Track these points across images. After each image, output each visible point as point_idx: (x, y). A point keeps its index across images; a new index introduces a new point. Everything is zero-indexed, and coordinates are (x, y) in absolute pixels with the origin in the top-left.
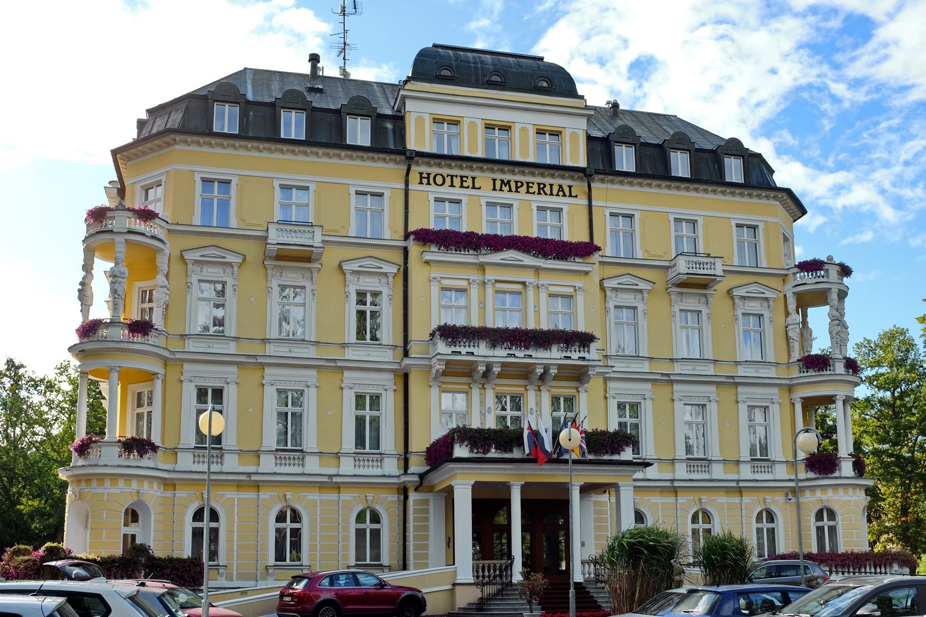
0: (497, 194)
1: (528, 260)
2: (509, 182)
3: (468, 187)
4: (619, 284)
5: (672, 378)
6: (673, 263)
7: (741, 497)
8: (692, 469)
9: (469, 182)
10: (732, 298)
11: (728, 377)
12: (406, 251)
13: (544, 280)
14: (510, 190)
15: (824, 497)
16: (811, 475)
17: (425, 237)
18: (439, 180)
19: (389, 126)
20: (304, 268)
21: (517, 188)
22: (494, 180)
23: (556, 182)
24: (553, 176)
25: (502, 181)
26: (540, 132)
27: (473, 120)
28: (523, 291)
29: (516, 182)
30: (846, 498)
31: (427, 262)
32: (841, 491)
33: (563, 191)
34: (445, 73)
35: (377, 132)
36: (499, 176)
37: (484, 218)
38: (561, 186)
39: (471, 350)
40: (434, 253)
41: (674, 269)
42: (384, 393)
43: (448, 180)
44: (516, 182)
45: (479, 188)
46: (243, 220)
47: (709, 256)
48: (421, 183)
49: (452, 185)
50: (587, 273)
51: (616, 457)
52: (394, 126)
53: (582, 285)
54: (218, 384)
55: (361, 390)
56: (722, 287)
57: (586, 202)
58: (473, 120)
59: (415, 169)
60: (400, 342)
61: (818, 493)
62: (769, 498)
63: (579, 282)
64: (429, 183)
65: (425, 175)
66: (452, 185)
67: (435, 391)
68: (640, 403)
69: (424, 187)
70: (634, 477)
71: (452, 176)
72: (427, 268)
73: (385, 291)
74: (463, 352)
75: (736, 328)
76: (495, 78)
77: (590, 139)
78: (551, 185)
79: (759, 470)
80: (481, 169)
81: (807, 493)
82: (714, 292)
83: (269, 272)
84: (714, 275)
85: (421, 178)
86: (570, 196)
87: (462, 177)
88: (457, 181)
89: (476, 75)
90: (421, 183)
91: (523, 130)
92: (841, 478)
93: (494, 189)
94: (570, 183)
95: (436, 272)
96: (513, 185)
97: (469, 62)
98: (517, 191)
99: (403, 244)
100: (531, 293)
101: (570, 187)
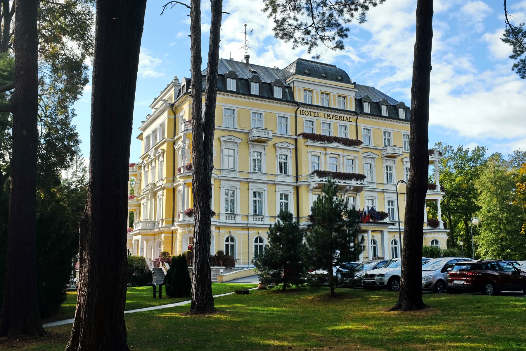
0: (326, 119)
1: (342, 146)
2: (330, 115)
3: (316, 116)
4: (227, 139)
5: (276, 182)
6: (251, 131)
7: (249, 231)
8: (256, 219)
9: (316, 115)
10: (275, 148)
11: (382, 190)
12: (296, 140)
13: (346, 153)
14: (330, 118)
15: (435, 236)
16: (430, 228)
17: (306, 136)
18: (307, 113)
19: (287, 90)
20: (262, 145)
21: (332, 117)
22: (325, 114)
23: (345, 116)
24: (344, 114)
25: (327, 115)
26: (305, 90)
27: (300, 88)
28: (338, 157)
29: (332, 115)
30: (442, 236)
31: (307, 146)
32: (440, 234)
33: (347, 119)
34: (307, 72)
35: (284, 93)
36: (326, 113)
37: (251, 118)
38: (347, 117)
39: (345, 181)
40: (309, 142)
41: (251, 134)
42: (290, 194)
43: (309, 113)
44: (332, 115)
45: (320, 117)
46: (240, 126)
47: (266, 129)
48: (300, 114)
49: (311, 115)
50: (359, 151)
51: (382, 221)
52: (289, 91)
53: (357, 156)
54: (286, 193)
55: (255, 191)
56: (271, 143)
57: (355, 124)
58: (300, 88)
59: (300, 108)
60: (295, 175)
61: (433, 235)
62: (261, 232)
63: (356, 155)
64: (303, 114)
65: (302, 111)
66: (311, 115)
67: (310, 194)
68: (262, 192)
69: (302, 116)
70: (388, 228)
71: (311, 112)
72: (306, 147)
73: (289, 155)
74: (324, 181)
75: (250, 157)
76: (323, 75)
77: (355, 99)
78: (344, 117)
79: (258, 219)
80: (321, 110)
81: (428, 234)
82: (268, 145)
83: (250, 146)
84: (269, 138)
85: (301, 112)
86: (350, 121)
87: (314, 112)
88: (312, 114)
89: (317, 73)
90: (300, 114)
91: (334, 95)
92: (439, 229)
93: (325, 118)
94: (350, 116)
95: (310, 149)
96: (331, 116)
97: (314, 68)
98: (332, 119)
99: (295, 137)
100: (341, 158)
101: (350, 118)
